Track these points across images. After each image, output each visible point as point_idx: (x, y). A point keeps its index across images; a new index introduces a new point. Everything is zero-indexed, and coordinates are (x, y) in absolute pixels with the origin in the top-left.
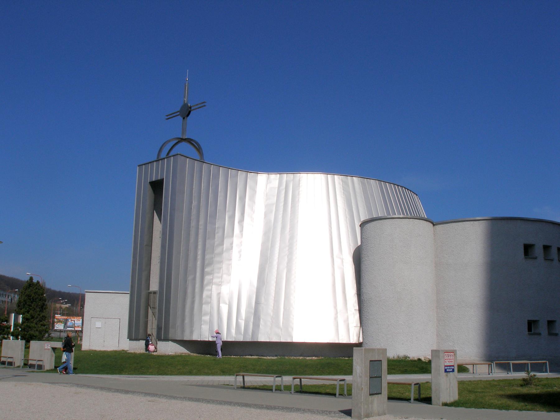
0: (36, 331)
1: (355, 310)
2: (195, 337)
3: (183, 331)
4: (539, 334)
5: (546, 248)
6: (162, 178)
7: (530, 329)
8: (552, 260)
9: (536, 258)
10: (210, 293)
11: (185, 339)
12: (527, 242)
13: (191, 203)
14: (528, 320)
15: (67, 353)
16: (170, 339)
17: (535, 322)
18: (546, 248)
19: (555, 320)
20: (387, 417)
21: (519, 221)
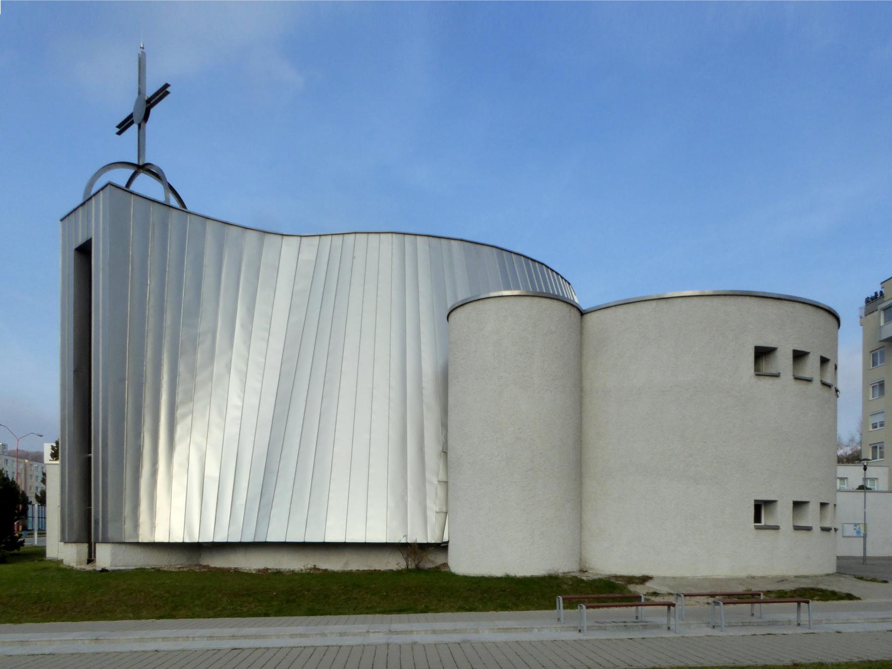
0: (32, 504)
1: (439, 481)
2: (161, 537)
3: (136, 526)
4: (776, 528)
5: (799, 356)
6: (89, 238)
7: (757, 519)
8: (809, 381)
9: (777, 376)
10: (871, 459)
11: (142, 539)
12: (762, 343)
13: (144, 284)
14: (756, 501)
15: (34, 545)
16: (111, 540)
17: (769, 503)
18: (799, 356)
19: (828, 502)
20: (136, 95)
21: (748, 299)
